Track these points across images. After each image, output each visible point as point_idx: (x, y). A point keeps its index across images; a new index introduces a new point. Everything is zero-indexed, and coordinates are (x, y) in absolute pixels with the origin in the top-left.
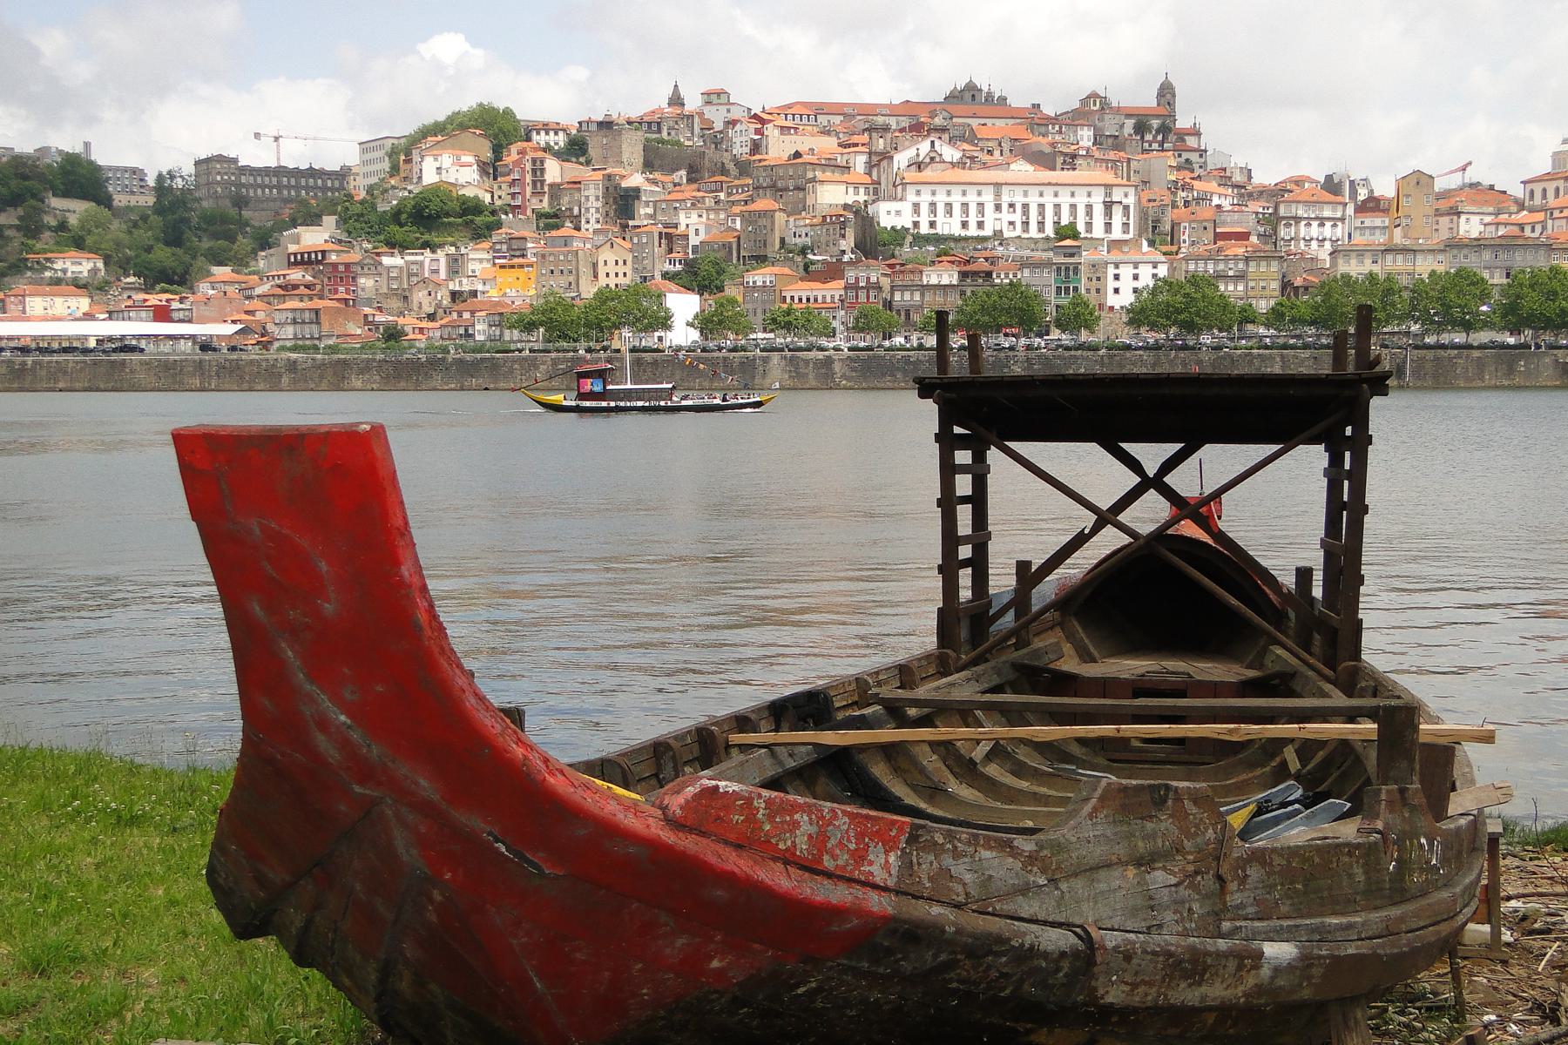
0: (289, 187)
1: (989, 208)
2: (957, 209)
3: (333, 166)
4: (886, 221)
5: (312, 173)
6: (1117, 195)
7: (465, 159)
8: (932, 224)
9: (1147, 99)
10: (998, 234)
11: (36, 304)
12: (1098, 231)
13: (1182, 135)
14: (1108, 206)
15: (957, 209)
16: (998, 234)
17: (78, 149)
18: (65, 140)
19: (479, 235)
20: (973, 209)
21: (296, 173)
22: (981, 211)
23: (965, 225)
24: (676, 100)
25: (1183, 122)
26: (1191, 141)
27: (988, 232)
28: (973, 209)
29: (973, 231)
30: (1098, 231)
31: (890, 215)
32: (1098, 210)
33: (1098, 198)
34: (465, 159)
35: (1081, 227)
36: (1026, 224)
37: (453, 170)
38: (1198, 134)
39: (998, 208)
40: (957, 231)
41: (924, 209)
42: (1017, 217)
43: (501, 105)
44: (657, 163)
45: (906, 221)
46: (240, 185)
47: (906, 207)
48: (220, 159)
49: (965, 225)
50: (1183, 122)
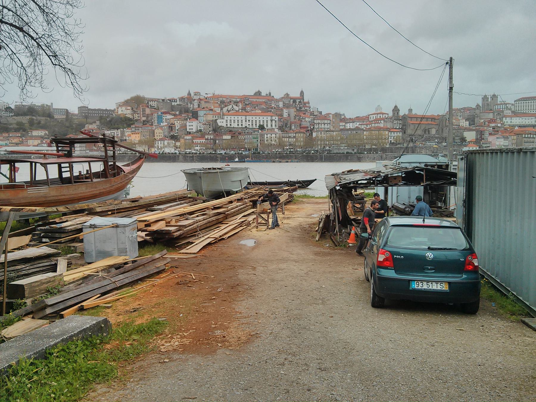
0: (101, 114)
1: (244, 121)
2: (236, 121)
3: (112, 109)
4: (220, 124)
5: (106, 110)
6: (274, 118)
7: (128, 108)
8: (231, 125)
9: (298, 95)
10: (246, 127)
11: (30, 142)
12: (269, 126)
13: (305, 103)
14: (272, 121)
15: (236, 121)
16: (246, 127)
17: (49, 104)
18: (134, 95)
19: (129, 126)
20: (240, 121)
21: (103, 110)
22: (242, 122)
23: (238, 125)
24: (189, 94)
25: (306, 100)
26: (307, 105)
27: (244, 126)
28: (240, 121)
29: (240, 126)
30: (269, 126)
31: (221, 123)
32: (269, 122)
33: (269, 118)
34: (128, 108)
35: (265, 126)
36: (252, 125)
37: (127, 112)
38: (309, 103)
39: (246, 121)
40: (236, 126)
41: (229, 121)
42: (250, 123)
43: (141, 95)
44: (174, 109)
45: (224, 125)
46: (88, 113)
47: (224, 121)
48: (84, 107)
49: (238, 125)
50: (306, 100)
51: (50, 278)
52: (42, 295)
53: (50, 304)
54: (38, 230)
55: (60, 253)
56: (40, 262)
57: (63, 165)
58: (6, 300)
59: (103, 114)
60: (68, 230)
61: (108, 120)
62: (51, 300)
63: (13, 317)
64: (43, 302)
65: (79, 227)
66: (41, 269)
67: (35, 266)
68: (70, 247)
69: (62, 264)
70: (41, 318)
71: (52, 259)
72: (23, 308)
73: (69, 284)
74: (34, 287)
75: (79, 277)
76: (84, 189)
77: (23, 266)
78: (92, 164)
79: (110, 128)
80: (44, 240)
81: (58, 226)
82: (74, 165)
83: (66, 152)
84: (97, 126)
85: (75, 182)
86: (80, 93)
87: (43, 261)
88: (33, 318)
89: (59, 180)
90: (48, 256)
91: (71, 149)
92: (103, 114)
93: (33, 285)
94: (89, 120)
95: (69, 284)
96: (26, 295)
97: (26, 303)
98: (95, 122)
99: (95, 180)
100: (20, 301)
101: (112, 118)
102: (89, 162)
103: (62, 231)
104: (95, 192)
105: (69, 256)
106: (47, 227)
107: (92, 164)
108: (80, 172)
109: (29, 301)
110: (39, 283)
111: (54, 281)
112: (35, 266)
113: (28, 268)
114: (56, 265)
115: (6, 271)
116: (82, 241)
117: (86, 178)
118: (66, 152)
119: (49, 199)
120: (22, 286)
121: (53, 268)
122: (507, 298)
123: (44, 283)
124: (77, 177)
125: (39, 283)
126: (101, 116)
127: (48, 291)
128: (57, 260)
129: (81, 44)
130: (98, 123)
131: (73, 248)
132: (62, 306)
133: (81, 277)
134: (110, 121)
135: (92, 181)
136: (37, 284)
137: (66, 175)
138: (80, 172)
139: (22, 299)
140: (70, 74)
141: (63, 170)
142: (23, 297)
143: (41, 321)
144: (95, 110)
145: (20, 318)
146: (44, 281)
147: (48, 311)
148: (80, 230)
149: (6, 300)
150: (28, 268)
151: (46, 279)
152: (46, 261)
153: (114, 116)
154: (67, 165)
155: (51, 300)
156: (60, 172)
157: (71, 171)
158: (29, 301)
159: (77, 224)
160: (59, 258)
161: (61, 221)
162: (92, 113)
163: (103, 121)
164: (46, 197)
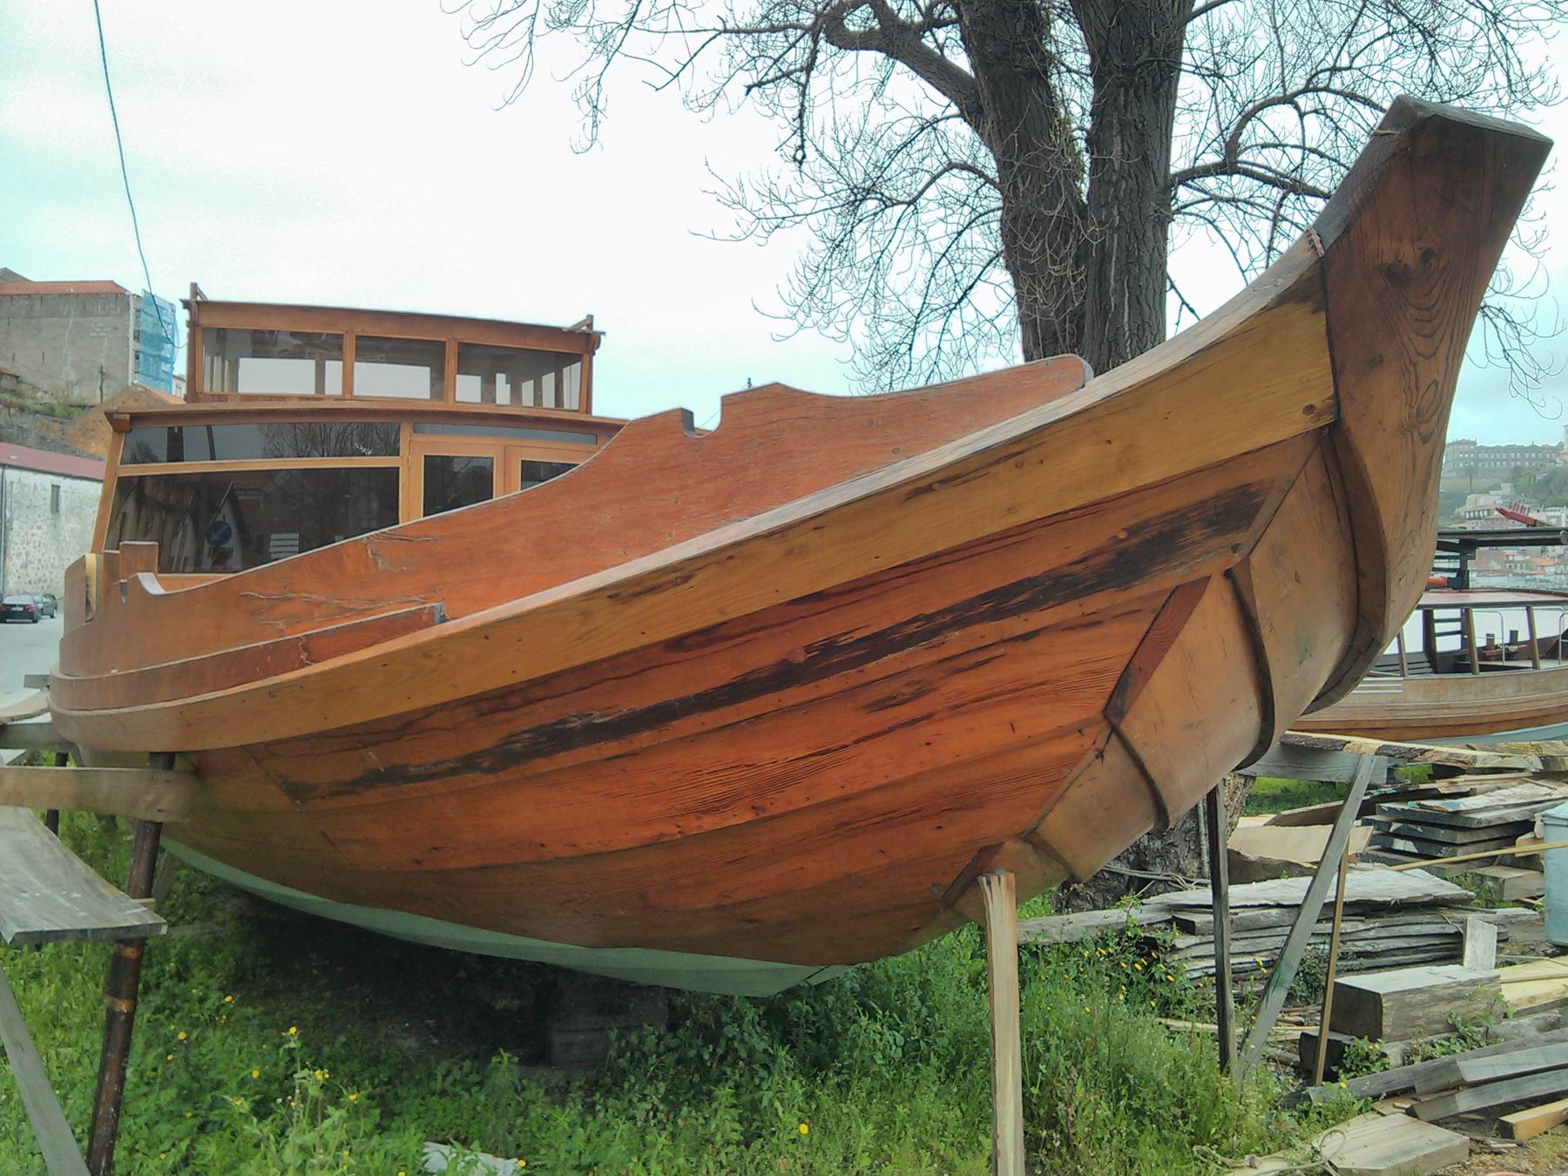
0: (1515, 460)
5: (1533, 448)
21: (1522, 449)
46: (1477, 460)
51: (1460, 984)
52: (1434, 1038)
53: (1470, 1077)
54: (1383, 812)
55: (1470, 899)
56: (1410, 918)
57: (1437, 614)
58: (1328, 1035)
59: (1523, 459)
60: (1480, 821)
61: (1539, 478)
62: (1475, 1067)
63: (1348, 1097)
64: (1451, 1067)
65: (1515, 815)
66: (1414, 943)
67: (1396, 931)
68: (1483, 877)
69: (1480, 939)
70: (1437, 1123)
71: (1447, 914)
72: (1376, 1068)
73: (1519, 1014)
74: (1413, 1006)
75: (1548, 995)
76: (1509, 691)
77: (1361, 926)
78: (1538, 613)
79: (1545, 504)
80: (1399, 844)
81: (1448, 805)
82: (1476, 614)
83: (1454, 575)
84: (1503, 497)
85: (1483, 668)
86: (1531, 382)
87: (1419, 918)
88: (1410, 1112)
89: (1424, 658)
90: (1433, 905)
91: (1464, 563)
92: (1523, 459)
93: (1408, 998)
94: (1478, 482)
95: (1519, 1014)
96: (1386, 1030)
97: (1384, 1055)
98: (1497, 487)
99: (1545, 665)
100: (1365, 1045)
101: (1554, 473)
102: (1528, 606)
103: (1457, 823)
104: (1544, 705)
105: (1500, 912)
106: (1411, 805)
107: (1538, 613)
108: (1490, 638)
109: (1394, 1051)
110: (1426, 996)
111: (1471, 998)
112: (1396, 931)
113: (1372, 934)
114: (1459, 938)
115: (1337, 937)
116: (1530, 862)
117: (1510, 656)
118: (1454, 575)
119: (1404, 715)
120: (1374, 999)
121: (1451, 949)
122: (1541, 1030)
123: (1441, 999)
124: (1483, 653)
125: (1426, 996)
126: (1517, 468)
127: (1453, 1028)
128: (1463, 922)
129: (1539, 226)
130: (1507, 488)
131: (1490, 884)
132: (1506, 1095)
133: (1555, 996)
134: (1547, 482)
135: (1535, 667)
136: (1419, 998)
137: (1447, 644)
138: (1490, 638)
139: (1373, 1040)
140: (1501, 322)
141: (1438, 628)
142: (1375, 1034)
143: (1442, 1136)
144: (1498, 449)
145: (1371, 1103)
146: (1440, 993)
147: (1465, 1102)
148: (1526, 826)
149: (1328, 1035)
150: (1372, 934)
151: (1447, 987)
152: (1427, 918)
153: (1560, 463)
154: (1456, 613)
155: (1475, 1067)
156: (1429, 636)
157: (1466, 631)
158: (1394, 1051)
159: (1506, 806)
160: (1470, 917)
161: (1454, 790)
162: (1495, 461)
163: (1522, 481)
164: (1393, 710)
